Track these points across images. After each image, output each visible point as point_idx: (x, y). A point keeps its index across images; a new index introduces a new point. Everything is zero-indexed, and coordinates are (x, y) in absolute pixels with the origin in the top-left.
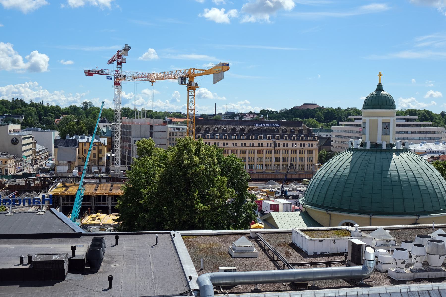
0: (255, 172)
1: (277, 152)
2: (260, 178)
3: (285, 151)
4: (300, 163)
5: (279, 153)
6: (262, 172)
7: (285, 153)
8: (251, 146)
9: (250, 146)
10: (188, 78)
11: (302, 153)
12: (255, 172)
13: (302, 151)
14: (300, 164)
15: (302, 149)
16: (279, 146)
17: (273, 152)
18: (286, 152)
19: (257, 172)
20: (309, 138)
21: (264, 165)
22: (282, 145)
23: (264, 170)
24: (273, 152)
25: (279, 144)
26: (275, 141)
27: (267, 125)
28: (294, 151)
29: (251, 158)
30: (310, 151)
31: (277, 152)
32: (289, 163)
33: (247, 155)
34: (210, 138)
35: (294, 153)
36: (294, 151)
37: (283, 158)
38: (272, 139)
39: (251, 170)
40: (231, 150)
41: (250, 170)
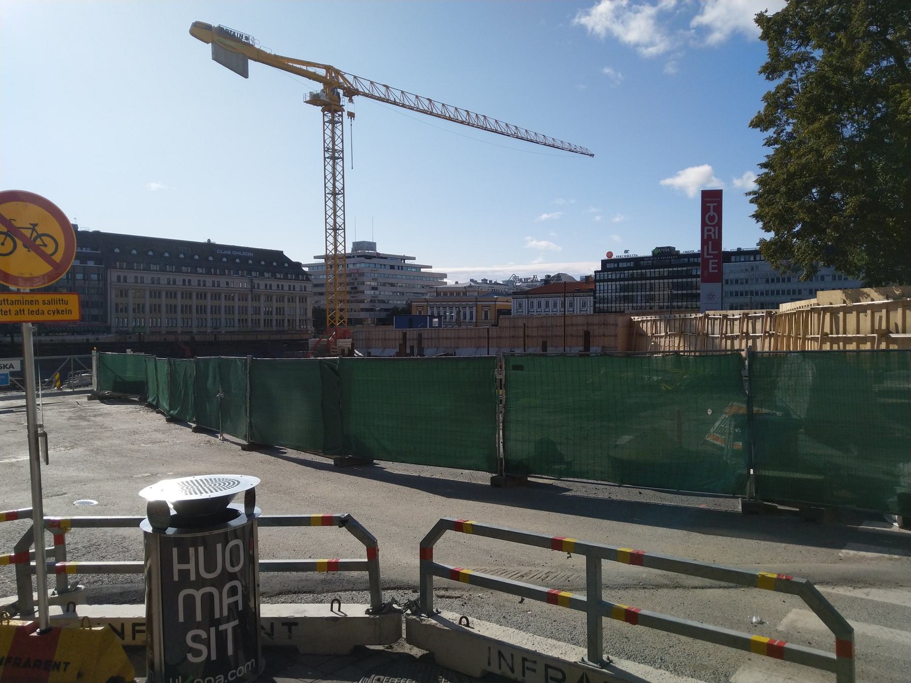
0: (223, 332)
1: (256, 298)
2: (258, 339)
3: (121, 291)
4: (254, 317)
5: (259, 300)
6: (233, 332)
7: (122, 296)
8: (290, 290)
9: (184, 284)
10: (620, 263)
11: (292, 302)
12: (223, 332)
13: (292, 297)
14: (289, 318)
15: (292, 293)
16: (258, 288)
17: (250, 297)
18: (269, 298)
19: (226, 332)
20: (289, 276)
21: (237, 321)
22: (262, 287)
23: (236, 329)
24: (250, 297)
25: (258, 285)
26: (252, 280)
27: (234, 253)
28: (155, 293)
29: (172, 309)
30: (215, 295)
31: (256, 298)
32: (237, 317)
33: (164, 301)
34: (142, 268)
35: (186, 298)
36: (155, 293)
37: (167, 305)
38: (247, 275)
39: (216, 329)
40: (180, 293)
41: (214, 329)
